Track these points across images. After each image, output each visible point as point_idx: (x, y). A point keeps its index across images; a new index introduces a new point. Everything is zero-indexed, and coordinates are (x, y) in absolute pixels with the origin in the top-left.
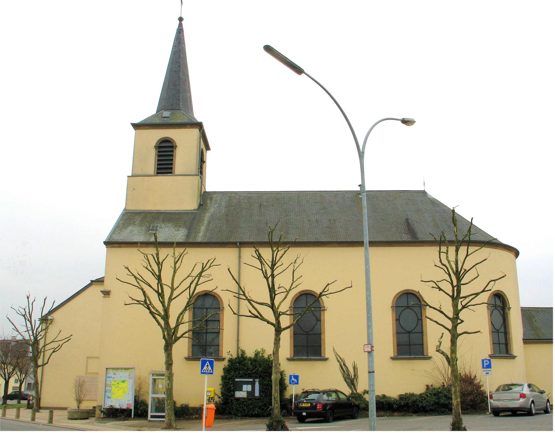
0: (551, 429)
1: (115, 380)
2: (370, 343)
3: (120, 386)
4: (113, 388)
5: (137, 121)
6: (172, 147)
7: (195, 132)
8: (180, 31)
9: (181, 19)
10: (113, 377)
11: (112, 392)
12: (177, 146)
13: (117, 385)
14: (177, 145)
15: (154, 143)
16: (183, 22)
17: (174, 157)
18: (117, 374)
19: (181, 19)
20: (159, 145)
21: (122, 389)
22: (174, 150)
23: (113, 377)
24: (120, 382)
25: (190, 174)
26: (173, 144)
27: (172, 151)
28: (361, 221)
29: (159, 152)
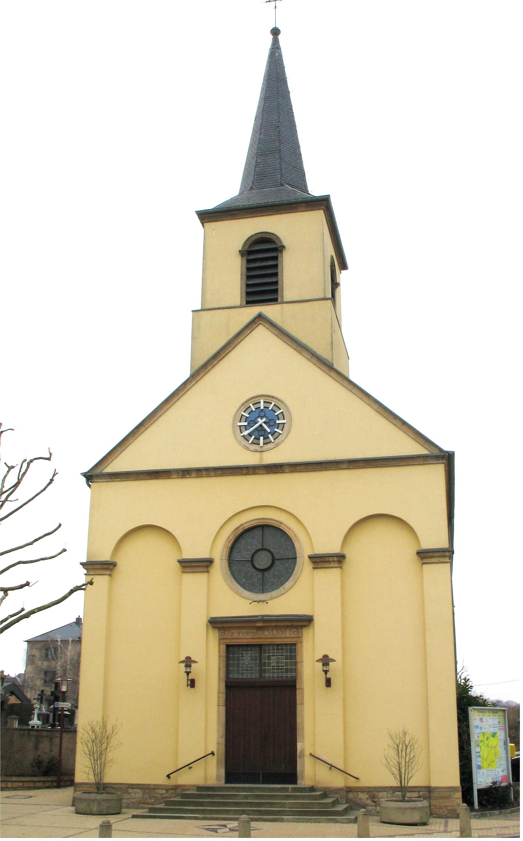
0: (453, 453)
1: (483, 733)
2: (325, 288)
3: (490, 744)
4: (483, 748)
5: (210, 205)
6: (276, 250)
7: (319, 215)
8: (275, 48)
9: (275, 32)
10: (480, 726)
11: (482, 756)
12: (284, 247)
13: (486, 742)
14: (284, 244)
15: (239, 244)
16: (280, 37)
17: (279, 277)
18: (484, 721)
19: (275, 32)
20: (249, 249)
21: (494, 748)
22: (279, 255)
23: (480, 726)
24: (489, 737)
25: (299, 299)
26: (276, 244)
27: (276, 258)
28: (189, 798)
29: (249, 261)
